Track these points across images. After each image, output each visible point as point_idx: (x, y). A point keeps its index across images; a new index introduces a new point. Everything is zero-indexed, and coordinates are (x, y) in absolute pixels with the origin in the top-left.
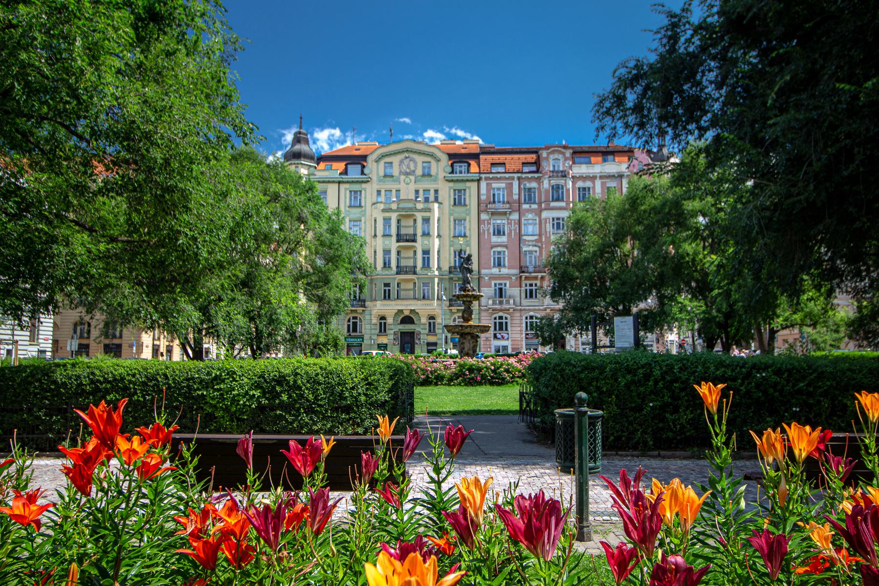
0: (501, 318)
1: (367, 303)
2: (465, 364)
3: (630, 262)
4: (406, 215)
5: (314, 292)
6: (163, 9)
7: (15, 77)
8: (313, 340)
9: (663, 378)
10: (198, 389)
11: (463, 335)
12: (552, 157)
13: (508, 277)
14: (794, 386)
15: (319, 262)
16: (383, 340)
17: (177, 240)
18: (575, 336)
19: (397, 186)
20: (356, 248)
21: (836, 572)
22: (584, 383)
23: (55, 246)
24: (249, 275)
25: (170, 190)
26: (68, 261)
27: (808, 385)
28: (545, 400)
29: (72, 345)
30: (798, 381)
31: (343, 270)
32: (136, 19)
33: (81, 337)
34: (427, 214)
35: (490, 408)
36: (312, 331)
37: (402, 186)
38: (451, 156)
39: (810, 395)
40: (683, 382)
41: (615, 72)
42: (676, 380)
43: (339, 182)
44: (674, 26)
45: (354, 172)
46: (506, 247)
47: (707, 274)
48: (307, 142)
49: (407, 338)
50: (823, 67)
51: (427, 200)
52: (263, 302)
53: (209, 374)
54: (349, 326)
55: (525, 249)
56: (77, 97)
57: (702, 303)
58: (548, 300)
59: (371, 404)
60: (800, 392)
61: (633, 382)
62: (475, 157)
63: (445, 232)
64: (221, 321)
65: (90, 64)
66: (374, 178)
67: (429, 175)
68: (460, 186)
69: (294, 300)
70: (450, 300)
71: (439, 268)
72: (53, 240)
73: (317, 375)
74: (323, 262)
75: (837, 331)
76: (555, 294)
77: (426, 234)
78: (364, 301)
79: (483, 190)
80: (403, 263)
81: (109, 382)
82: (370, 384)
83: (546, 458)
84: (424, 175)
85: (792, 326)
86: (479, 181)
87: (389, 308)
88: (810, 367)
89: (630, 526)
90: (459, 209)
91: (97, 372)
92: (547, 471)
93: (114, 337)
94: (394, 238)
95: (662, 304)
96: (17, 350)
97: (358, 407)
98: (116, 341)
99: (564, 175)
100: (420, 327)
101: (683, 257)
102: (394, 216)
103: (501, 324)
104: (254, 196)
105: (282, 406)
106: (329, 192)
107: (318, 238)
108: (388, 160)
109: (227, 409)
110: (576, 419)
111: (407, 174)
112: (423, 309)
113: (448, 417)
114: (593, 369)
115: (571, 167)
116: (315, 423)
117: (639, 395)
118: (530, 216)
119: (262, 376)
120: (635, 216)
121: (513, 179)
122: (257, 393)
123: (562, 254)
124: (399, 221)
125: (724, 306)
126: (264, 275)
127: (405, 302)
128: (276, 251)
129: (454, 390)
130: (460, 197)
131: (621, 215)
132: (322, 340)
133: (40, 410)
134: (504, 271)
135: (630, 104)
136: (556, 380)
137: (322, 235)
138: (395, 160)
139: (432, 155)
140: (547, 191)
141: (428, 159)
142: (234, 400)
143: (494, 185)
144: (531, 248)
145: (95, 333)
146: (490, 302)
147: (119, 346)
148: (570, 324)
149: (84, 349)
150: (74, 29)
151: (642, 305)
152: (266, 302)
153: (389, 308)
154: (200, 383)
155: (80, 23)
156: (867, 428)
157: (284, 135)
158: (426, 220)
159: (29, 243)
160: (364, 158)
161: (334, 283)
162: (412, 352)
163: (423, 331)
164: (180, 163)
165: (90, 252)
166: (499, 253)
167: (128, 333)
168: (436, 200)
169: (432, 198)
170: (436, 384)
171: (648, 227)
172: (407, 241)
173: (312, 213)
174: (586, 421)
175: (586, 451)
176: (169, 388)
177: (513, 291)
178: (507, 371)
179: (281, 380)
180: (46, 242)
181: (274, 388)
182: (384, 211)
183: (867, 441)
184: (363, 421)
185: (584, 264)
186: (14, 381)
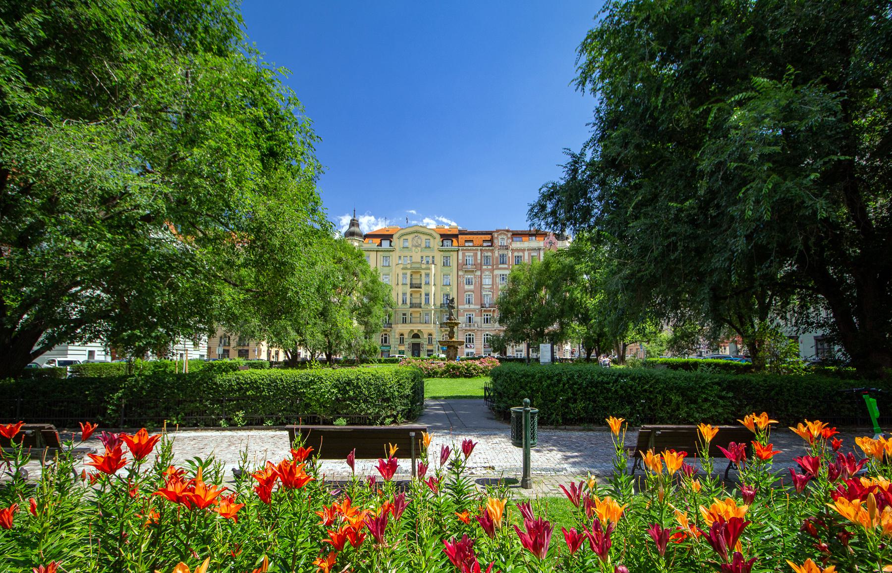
0: (470, 335)
2: (450, 365)
3: (544, 302)
4: (416, 272)
5: (363, 319)
6: (278, 150)
7: (192, 194)
8: (362, 348)
9: (568, 382)
10: (301, 388)
11: (449, 347)
12: (500, 237)
13: (474, 310)
14: (642, 387)
15: (365, 301)
16: (402, 348)
17: (287, 293)
18: (513, 347)
19: (411, 254)
20: (387, 292)
21: (691, 543)
22: (523, 385)
23: (213, 296)
24: (324, 308)
25: (283, 264)
26: (221, 306)
27: (651, 387)
28: (500, 394)
29: (219, 350)
30: (644, 384)
31: (379, 306)
32: (262, 155)
33: (225, 345)
34: (427, 271)
35: (465, 395)
36: (360, 343)
37: (413, 254)
38: (442, 236)
39: (651, 392)
40: (579, 385)
41: (540, 190)
42: (575, 383)
43: (377, 251)
44: (576, 162)
45: (385, 244)
46: (473, 292)
47: (588, 310)
48: (358, 225)
49: (416, 347)
50: (661, 191)
51: (428, 262)
52: (333, 325)
53: (307, 379)
55: (484, 293)
56: (228, 206)
57: (585, 328)
58: (497, 325)
59: (401, 397)
60: (645, 391)
61: (551, 384)
62: (456, 236)
63: (438, 283)
64: (308, 337)
65: (237, 186)
66: (397, 248)
67: (429, 247)
68: (447, 254)
69: (351, 324)
70: (441, 324)
71: (434, 304)
72: (211, 292)
73: (370, 379)
74: (367, 300)
75: (661, 346)
76: (501, 321)
77: (427, 284)
79: (460, 257)
80: (414, 301)
81: (248, 384)
82: (400, 385)
83: (501, 430)
84: (426, 247)
85: (636, 342)
86: (458, 251)
87: (405, 329)
88: (651, 376)
89: (594, 546)
90: (446, 268)
91: (241, 377)
92: (503, 440)
93: (244, 345)
94: (409, 286)
95: (562, 328)
96: (187, 354)
97: (393, 398)
98: (246, 348)
99: (507, 248)
100: (424, 341)
101: (575, 300)
102: (409, 272)
103: (470, 338)
104: (330, 265)
105: (351, 399)
106: (371, 257)
107: (365, 286)
108: (405, 237)
109: (318, 400)
110: (523, 415)
111: (416, 246)
112: (425, 329)
113: (443, 401)
114: (528, 376)
115: (511, 244)
116: (369, 409)
117: (554, 392)
118: (487, 273)
119: (338, 380)
120: (548, 274)
121: (477, 250)
122: (335, 391)
123: (506, 297)
124: (411, 275)
125: (598, 329)
126: (334, 308)
127: (415, 325)
128: (340, 293)
129: (444, 380)
130: (447, 261)
131: (540, 273)
132: (367, 348)
133: (207, 401)
134: (472, 307)
135: (549, 210)
136: (507, 382)
137: (367, 284)
138: (410, 237)
139: (430, 235)
140: (497, 258)
141: (428, 237)
142: (322, 395)
143: (467, 254)
144: (487, 293)
145: (233, 344)
146: (464, 325)
147: (247, 351)
148: (509, 340)
149: (226, 353)
150: (227, 164)
151: (551, 328)
152: (335, 325)
153: (405, 329)
154: (302, 384)
155: (230, 159)
156: (704, 446)
157: (341, 220)
158: (427, 275)
159: (197, 293)
160: (391, 236)
161: (374, 313)
162: (419, 356)
163: (425, 343)
164: (290, 247)
165: (234, 299)
166: (469, 295)
167: (252, 343)
168: (433, 263)
169: (430, 262)
170: (434, 377)
171: (555, 281)
172: (416, 288)
173: (361, 270)
174: (529, 416)
175: (529, 435)
176: (284, 387)
177: (477, 319)
178: (474, 369)
179: (349, 383)
180: (208, 293)
181: (345, 387)
182: (403, 269)
183: (704, 454)
184: (396, 407)
185: (519, 303)
186: (191, 383)
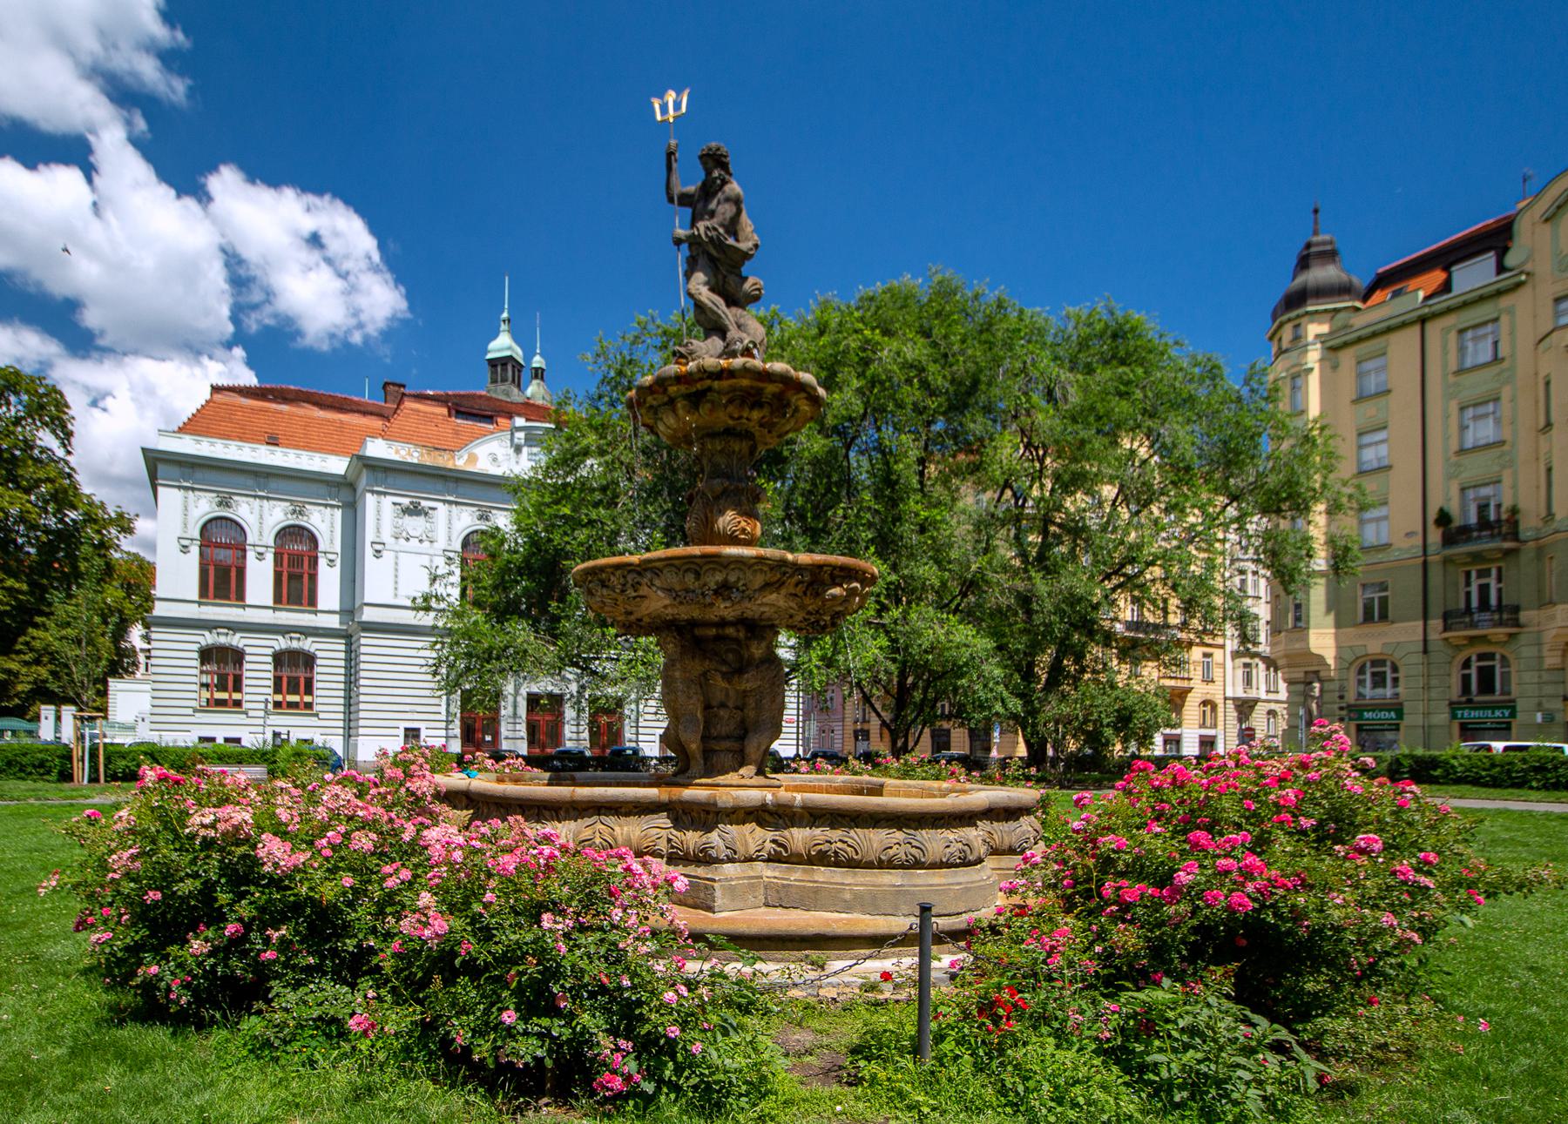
1: (1524, 616)
33: (1203, 725)
54: (1466, 680)
78: (1516, 609)
